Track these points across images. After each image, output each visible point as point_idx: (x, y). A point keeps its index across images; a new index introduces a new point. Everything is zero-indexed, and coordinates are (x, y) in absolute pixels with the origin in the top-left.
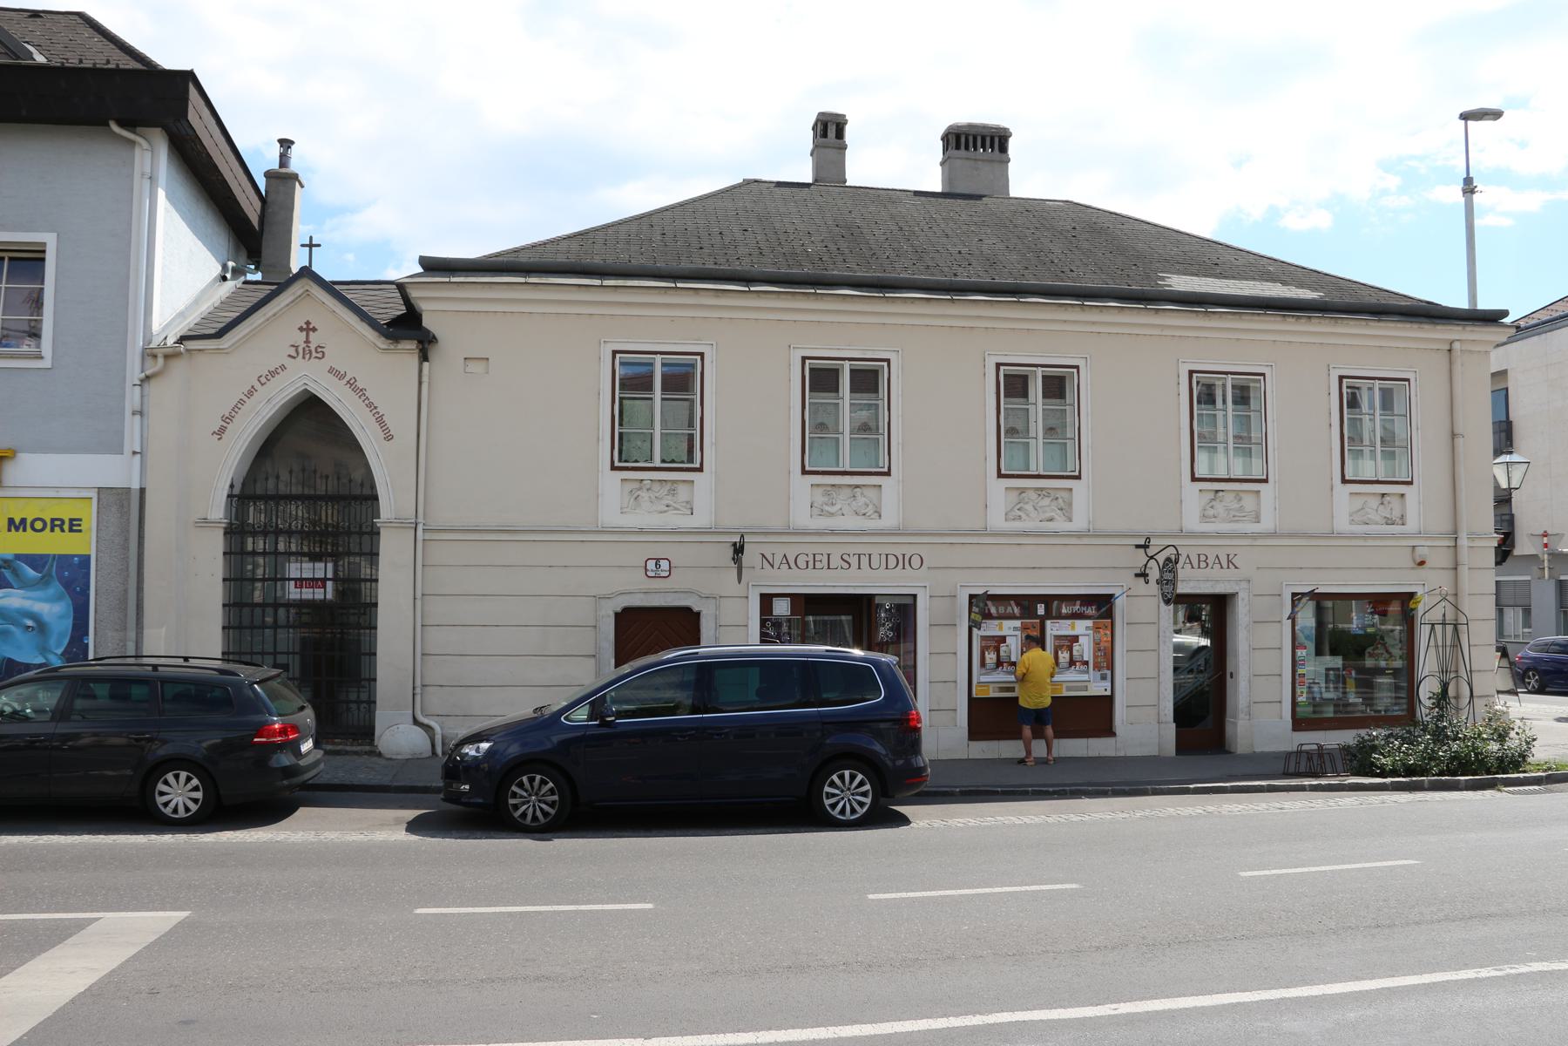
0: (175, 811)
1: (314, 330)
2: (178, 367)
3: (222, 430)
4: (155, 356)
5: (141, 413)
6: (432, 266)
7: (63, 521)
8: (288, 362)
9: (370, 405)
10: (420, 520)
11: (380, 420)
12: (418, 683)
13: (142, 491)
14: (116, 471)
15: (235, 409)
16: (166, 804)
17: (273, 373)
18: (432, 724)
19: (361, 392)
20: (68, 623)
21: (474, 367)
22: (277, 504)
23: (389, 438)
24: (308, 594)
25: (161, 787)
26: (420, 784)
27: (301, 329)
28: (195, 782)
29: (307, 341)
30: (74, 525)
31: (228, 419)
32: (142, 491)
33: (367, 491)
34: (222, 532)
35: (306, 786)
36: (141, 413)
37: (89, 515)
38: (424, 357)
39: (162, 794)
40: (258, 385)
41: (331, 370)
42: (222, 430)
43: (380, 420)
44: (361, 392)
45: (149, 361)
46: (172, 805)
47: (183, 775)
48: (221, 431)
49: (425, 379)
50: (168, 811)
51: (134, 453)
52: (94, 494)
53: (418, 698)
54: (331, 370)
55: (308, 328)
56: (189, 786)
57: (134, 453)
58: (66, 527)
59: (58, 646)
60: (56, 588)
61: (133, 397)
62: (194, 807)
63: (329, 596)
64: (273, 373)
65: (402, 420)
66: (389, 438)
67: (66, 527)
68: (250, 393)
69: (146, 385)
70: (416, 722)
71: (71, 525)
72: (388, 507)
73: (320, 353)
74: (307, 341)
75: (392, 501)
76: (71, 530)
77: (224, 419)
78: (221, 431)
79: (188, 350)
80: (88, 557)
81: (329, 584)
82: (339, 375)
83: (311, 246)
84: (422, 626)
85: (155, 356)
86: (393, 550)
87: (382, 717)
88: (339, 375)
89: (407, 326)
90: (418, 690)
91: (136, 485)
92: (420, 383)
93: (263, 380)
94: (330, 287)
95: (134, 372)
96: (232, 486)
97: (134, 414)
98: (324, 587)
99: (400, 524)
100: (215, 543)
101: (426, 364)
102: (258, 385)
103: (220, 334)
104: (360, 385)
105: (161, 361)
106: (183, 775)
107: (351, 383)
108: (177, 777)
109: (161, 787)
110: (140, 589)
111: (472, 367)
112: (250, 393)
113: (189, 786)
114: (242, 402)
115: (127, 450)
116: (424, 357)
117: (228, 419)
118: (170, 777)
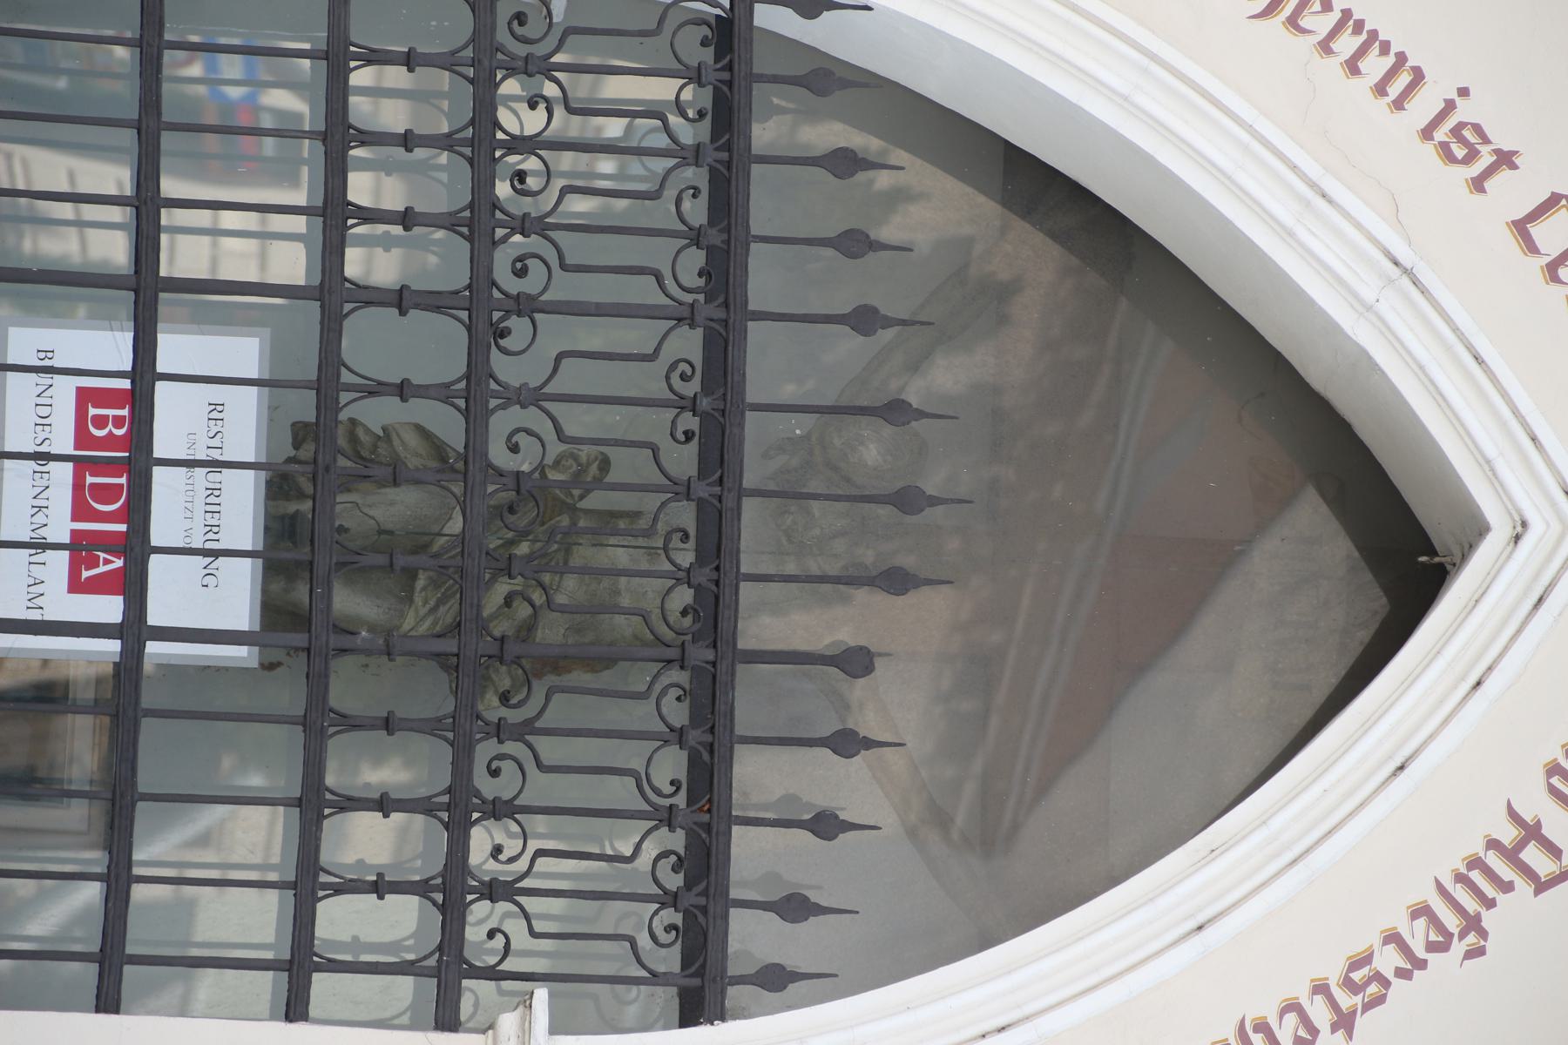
33: (751, 937)
114: (1402, 80)
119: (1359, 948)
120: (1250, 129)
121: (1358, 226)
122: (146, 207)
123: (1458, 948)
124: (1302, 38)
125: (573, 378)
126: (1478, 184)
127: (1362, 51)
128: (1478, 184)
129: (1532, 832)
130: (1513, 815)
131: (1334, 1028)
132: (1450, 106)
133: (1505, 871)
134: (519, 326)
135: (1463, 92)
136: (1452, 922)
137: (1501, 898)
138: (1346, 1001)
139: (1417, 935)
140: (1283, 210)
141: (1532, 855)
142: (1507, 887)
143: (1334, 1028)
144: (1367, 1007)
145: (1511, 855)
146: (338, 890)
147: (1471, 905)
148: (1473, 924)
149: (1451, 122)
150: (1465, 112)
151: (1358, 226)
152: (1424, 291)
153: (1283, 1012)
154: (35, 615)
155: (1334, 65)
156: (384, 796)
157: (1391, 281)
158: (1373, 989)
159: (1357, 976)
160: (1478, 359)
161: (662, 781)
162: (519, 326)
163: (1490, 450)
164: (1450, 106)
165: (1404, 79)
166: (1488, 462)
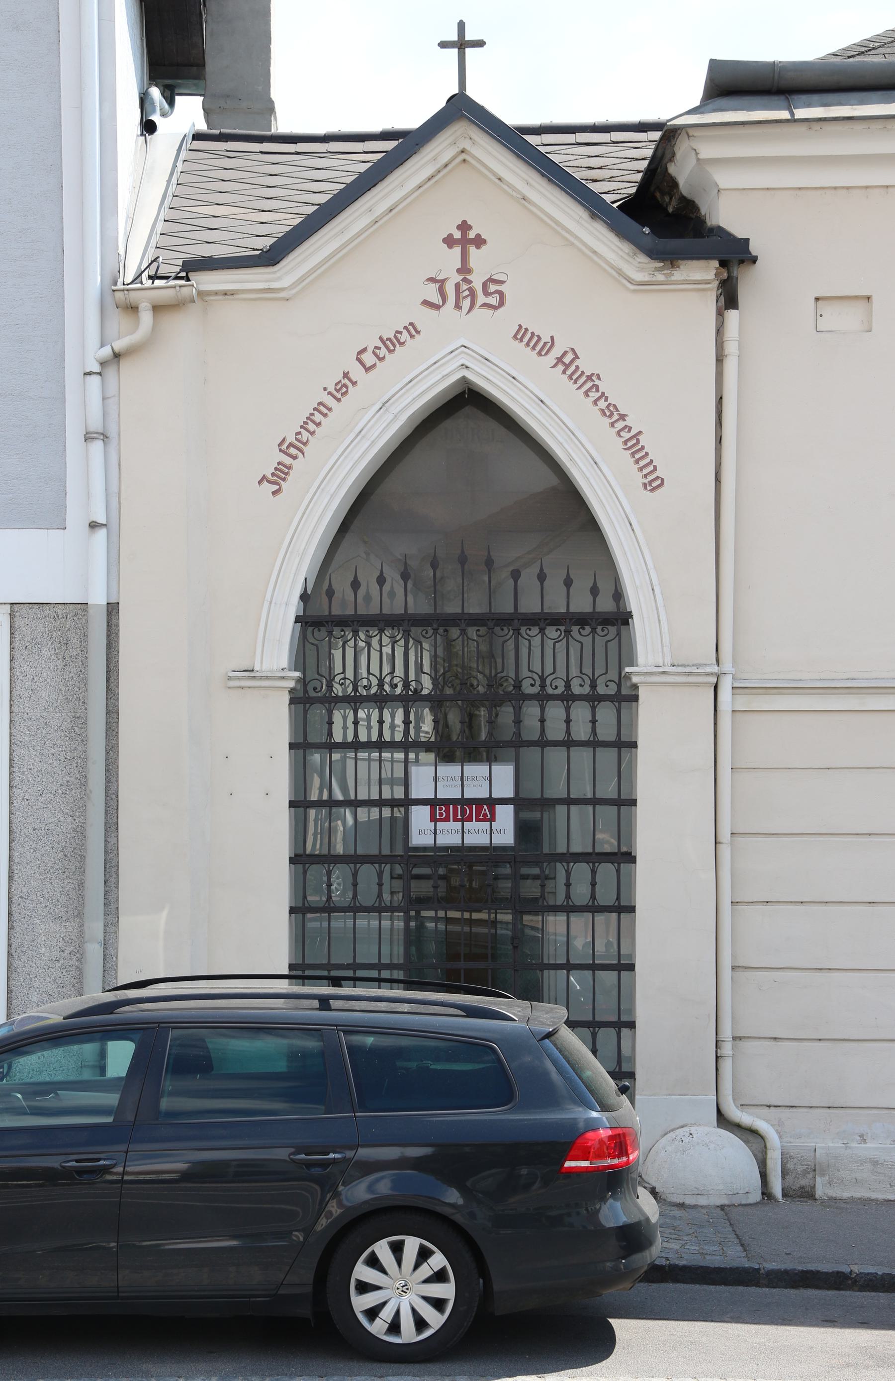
0: (394, 1327)
1: (479, 242)
2: (183, 329)
3: (281, 474)
4: (132, 309)
5: (105, 437)
6: (732, 84)
8: (424, 318)
9: (612, 413)
10: (727, 665)
11: (634, 445)
12: (727, 1033)
13: (112, 609)
15: (310, 424)
16: (373, 1313)
17: (391, 343)
18: (762, 1125)
19: (589, 383)
21: (837, 318)
23: (654, 484)
24: (450, 834)
25: (362, 1272)
26: (826, 1267)
27: (449, 241)
28: (438, 1260)
29: (465, 269)
31: (293, 448)
32: (112, 609)
33: (605, 605)
34: (286, 698)
35: (662, 1273)
36: (105, 437)
38: (729, 298)
39: (364, 1288)
40: (357, 372)
41: (520, 334)
42: (281, 474)
43: (634, 445)
44: (589, 383)
45: (117, 320)
46: (387, 1314)
47: (412, 1244)
48: (278, 477)
49: (731, 348)
50: (378, 1328)
51: (93, 525)
53: (727, 1066)
54: (520, 334)
55: (465, 239)
56: (425, 1271)
57: (93, 525)
61: (83, 402)
62: (436, 1320)
64: (391, 343)
65: (682, 448)
66: (654, 484)
68: (341, 389)
69: (111, 372)
70: (723, 1120)
72: (653, 642)
73: (495, 294)
74: (465, 269)
77: (284, 447)
78: (278, 477)
79: (200, 294)
82: (540, 346)
83: (462, 45)
84: (729, 905)
85: (132, 309)
86: (668, 741)
88: (540, 346)
89: (662, 215)
90: (727, 1049)
91: (98, 598)
92: (720, 360)
93: (369, 358)
94: (515, 140)
95: (84, 336)
97: (88, 437)
99: (681, 675)
100: (270, 723)
101: (732, 315)
102: (357, 372)
103: (270, 257)
104: (586, 365)
105: (146, 317)
106: (412, 1244)
107: (567, 363)
108: (397, 1249)
109: (362, 1272)
110: (111, 826)
111: (833, 317)
112: (341, 389)
113: (425, 1271)
115: (75, 518)
116: (729, 298)
117: (293, 448)
118: (382, 1249)
119: (599, 413)
128: (354, 383)
129: (560, 360)
132: (329, 393)
133: (573, 368)
136: (589, 384)
139: (594, 395)
141: (567, 360)
144: (617, 410)
145: (567, 366)
147: (584, 379)
148: (589, 378)
151: (369, 421)
158: (611, 408)
159: (608, 414)
163: (440, 376)
164: (329, 393)
165: (321, 408)
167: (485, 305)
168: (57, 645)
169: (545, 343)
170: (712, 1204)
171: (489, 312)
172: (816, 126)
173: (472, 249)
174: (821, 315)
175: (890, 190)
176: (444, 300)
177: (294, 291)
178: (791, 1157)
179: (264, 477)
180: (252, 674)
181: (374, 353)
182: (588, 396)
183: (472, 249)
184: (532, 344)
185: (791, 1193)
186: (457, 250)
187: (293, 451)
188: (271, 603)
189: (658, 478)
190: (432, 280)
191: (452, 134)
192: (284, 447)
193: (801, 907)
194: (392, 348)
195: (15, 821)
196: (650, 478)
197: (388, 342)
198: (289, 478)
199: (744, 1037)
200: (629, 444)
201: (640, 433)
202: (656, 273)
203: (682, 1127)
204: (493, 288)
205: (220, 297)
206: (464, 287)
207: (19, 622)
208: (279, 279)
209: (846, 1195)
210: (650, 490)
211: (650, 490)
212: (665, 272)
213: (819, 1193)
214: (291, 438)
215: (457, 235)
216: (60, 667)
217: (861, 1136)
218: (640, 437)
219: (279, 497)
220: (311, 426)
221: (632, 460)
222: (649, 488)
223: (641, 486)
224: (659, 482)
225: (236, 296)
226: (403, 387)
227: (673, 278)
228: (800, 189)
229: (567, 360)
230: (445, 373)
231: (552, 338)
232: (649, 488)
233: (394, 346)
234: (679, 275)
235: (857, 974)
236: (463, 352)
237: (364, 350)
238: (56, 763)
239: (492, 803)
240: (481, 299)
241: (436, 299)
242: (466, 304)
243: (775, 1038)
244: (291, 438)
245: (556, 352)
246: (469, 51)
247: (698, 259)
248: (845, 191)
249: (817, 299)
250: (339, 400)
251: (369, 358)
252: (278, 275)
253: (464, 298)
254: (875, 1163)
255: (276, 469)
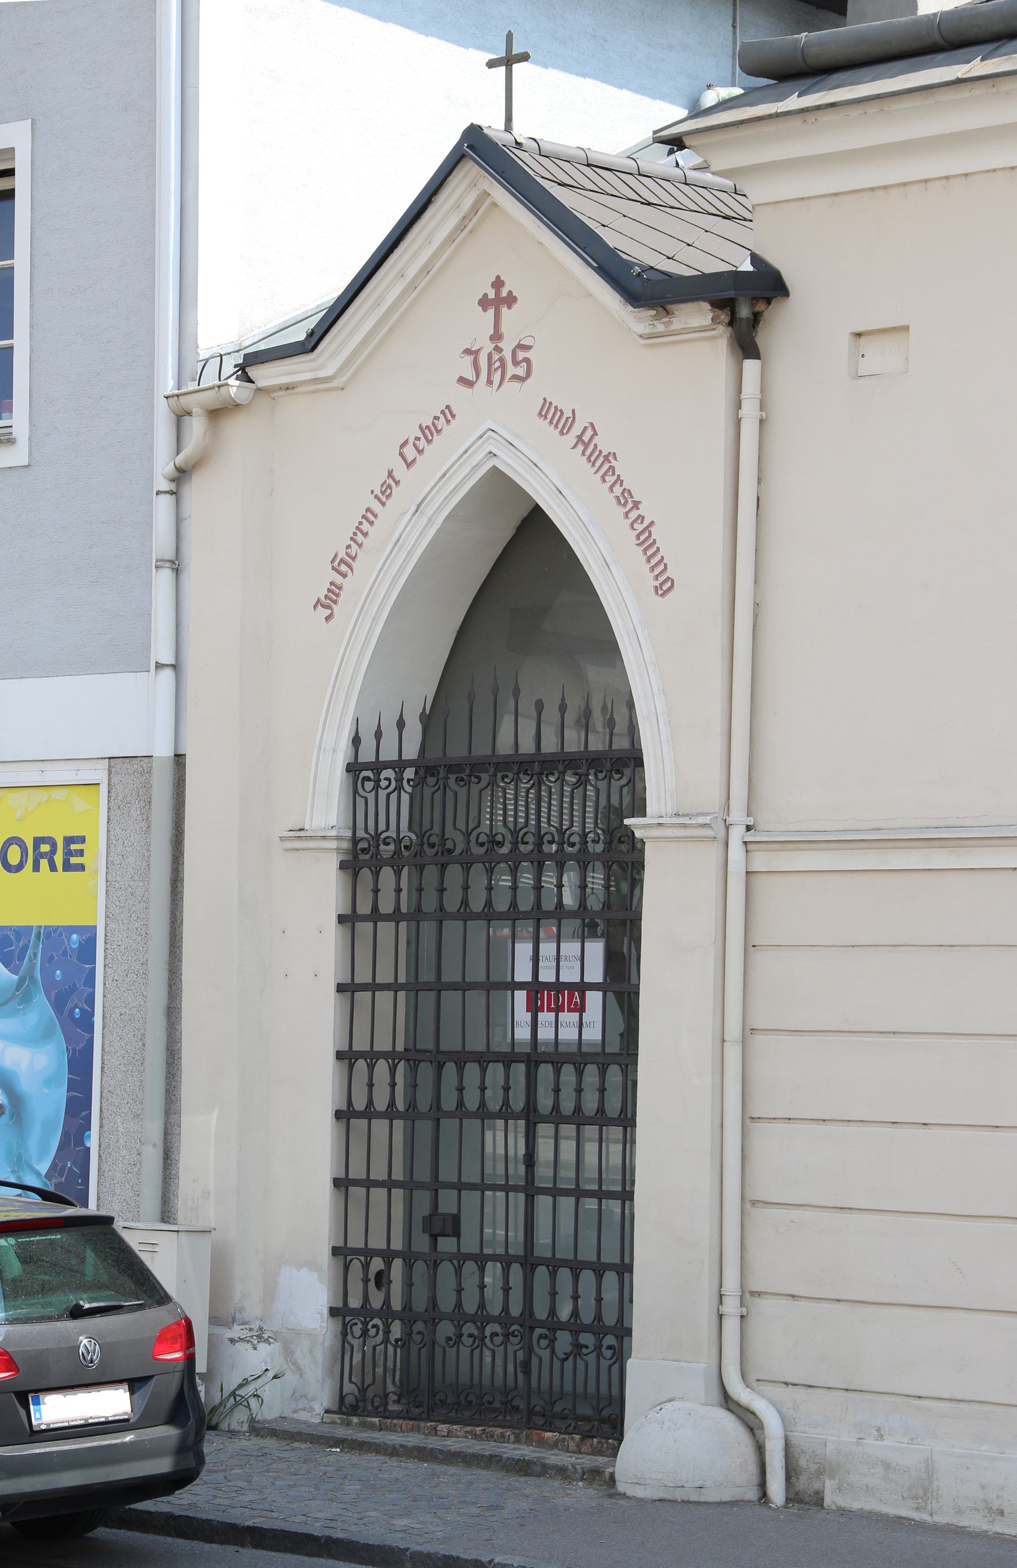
2: (237, 431)
3: (334, 592)
7: (51, 841)
8: (459, 397)
9: (628, 501)
10: (738, 816)
13: (179, 759)
14: (125, 714)
17: (429, 432)
19: (604, 463)
20: (61, 1094)
21: (878, 357)
22: (582, 782)
23: (664, 587)
27: (484, 303)
29: (496, 336)
30: (64, 854)
31: (343, 564)
32: (179, 759)
33: (621, 743)
34: (332, 862)
37: (91, 820)
41: (548, 411)
42: (334, 592)
44: (604, 463)
52: (99, 774)
53: (732, 1326)
54: (548, 411)
55: (498, 300)
57: (159, 666)
58: (59, 859)
59: (41, 1158)
60: (40, 1009)
63: (593, 1034)
64: (429, 432)
66: (664, 587)
67: (59, 859)
70: (727, 1401)
71: (68, 854)
74: (496, 336)
75: (677, 771)
76: (67, 867)
80: (94, 928)
81: (594, 1000)
87: (642, 1376)
90: (731, 1306)
91: (163, 750)
93: (410, 452)
96: (356, 741)
98: (581, 1009)
99: (687, 825)
102: (400, 471)
104: (604, 443)
114: (369, 516)
117: (343, 564)
119: (614, 501)
120: (380, 571)
121: (406, 527)
122: (464, 987)
123: (614, 463)
124: (358, 555)
125: (461, 824)
126: (397, 483)
127: (361, 531)
128: (397, 483)
129: (580, 438)
130: (574, 447)
131: (638, 509)
132: (376, 497)
133: (592, 447)
134: (449, 845)
135: (372, 492)
136: (606, 466)
137: (599, 448)
138: (630, 505)
139: (611, 479)
140: (403, 555)
141: (586, 438)
142: (596, 446)
143: (638, 509)
144: (632, 497)
145: (586, 445)
146: (467, 905)
147: (601, 459)
148: (606, 458)
149: (380, 495)
150: (377, 492)
151: (406, 527)
152: (424, 499)
153: (634, 529)
154: (554, 1025)
155: (366, 542)
156: (580, 887)
157: (422, 513)
158: (626, 495)
159: (623, 502)
160: (444, 475)
161: (574, 780)
162: (449, 845)
163: (469, 468)
164: (376, 497)
165: (369, 515)
166: (472, 469)
167: (515, 377)
168: (142, 804)
169: (567, 419)
170: (649, 1497)
171: (516, 385)
172: (811, 117)
173: (504, 310)
174: (863, 356)
175: (929, 184)
176: (478, 376)
177: (344, 379)
178: (803, 1452)
179: (319, 600)
180: (302, 834)
181: (414, 445)
182: (604, 481)
183: (504, 310)
184: (555, 422)
185: (807, 1499)
186: (491, 311)
187: (344, 568)
188: (320, 748)
189: (668, 578)
190: (467, 352)
191: (465, 176)
192: (336, 564)
193: (822, 1127)
194: (430, 438)
195: (107, 1004)
196: (661, 579)
197: (427, 431)
198: (340, 600)
199: (766, 1293)
200: (642, 538)
201: (652, 523)
202: (656, 323)
203: (670, 1401)
204: (521, 355)
205: (282, 393)
206: (496, 357)
207: (115, 779)
208: (322, 366)
209: (856, 1506)
210: (661, 595)
211: (661, 595)
212: (664, 320)
213: (828, 1501)
214: (342, 554)
215: (492, 295)
216: (144, 829)
217: (878, 1430)
218: (652, 529)
219: (332, 622)
220: (360, 538)
221: (645, 558)
222: (660, 592)
223: (653, 590)
224: (669, 584)
225: (296, 390)
226: (435, 485)
227: (673, 327)
228: (836, 194)
229: (586, 438)
230: (474, 464)
231: (573, 411)
232: (660, 592)
233: (432, 435)
234: (677, 324)
235: (878, 1217)
236: (490, 437)
237: (406, 442)
238: (139, 938)
239: (583, 987)
240: (511, 370)
241: (470, 375)
242: (497, 377)
243: (793, 1296)
244: (342, 554)
245: (577, 430)
246: (516, 67)
247: (693, 300)
248: (882, 192)
249: (859, 335)
250: (383, 504)
251: (410, 452)
252: (320, 361)
253: (496, 370)
254: (887, 1466)
255: (329, 590)
